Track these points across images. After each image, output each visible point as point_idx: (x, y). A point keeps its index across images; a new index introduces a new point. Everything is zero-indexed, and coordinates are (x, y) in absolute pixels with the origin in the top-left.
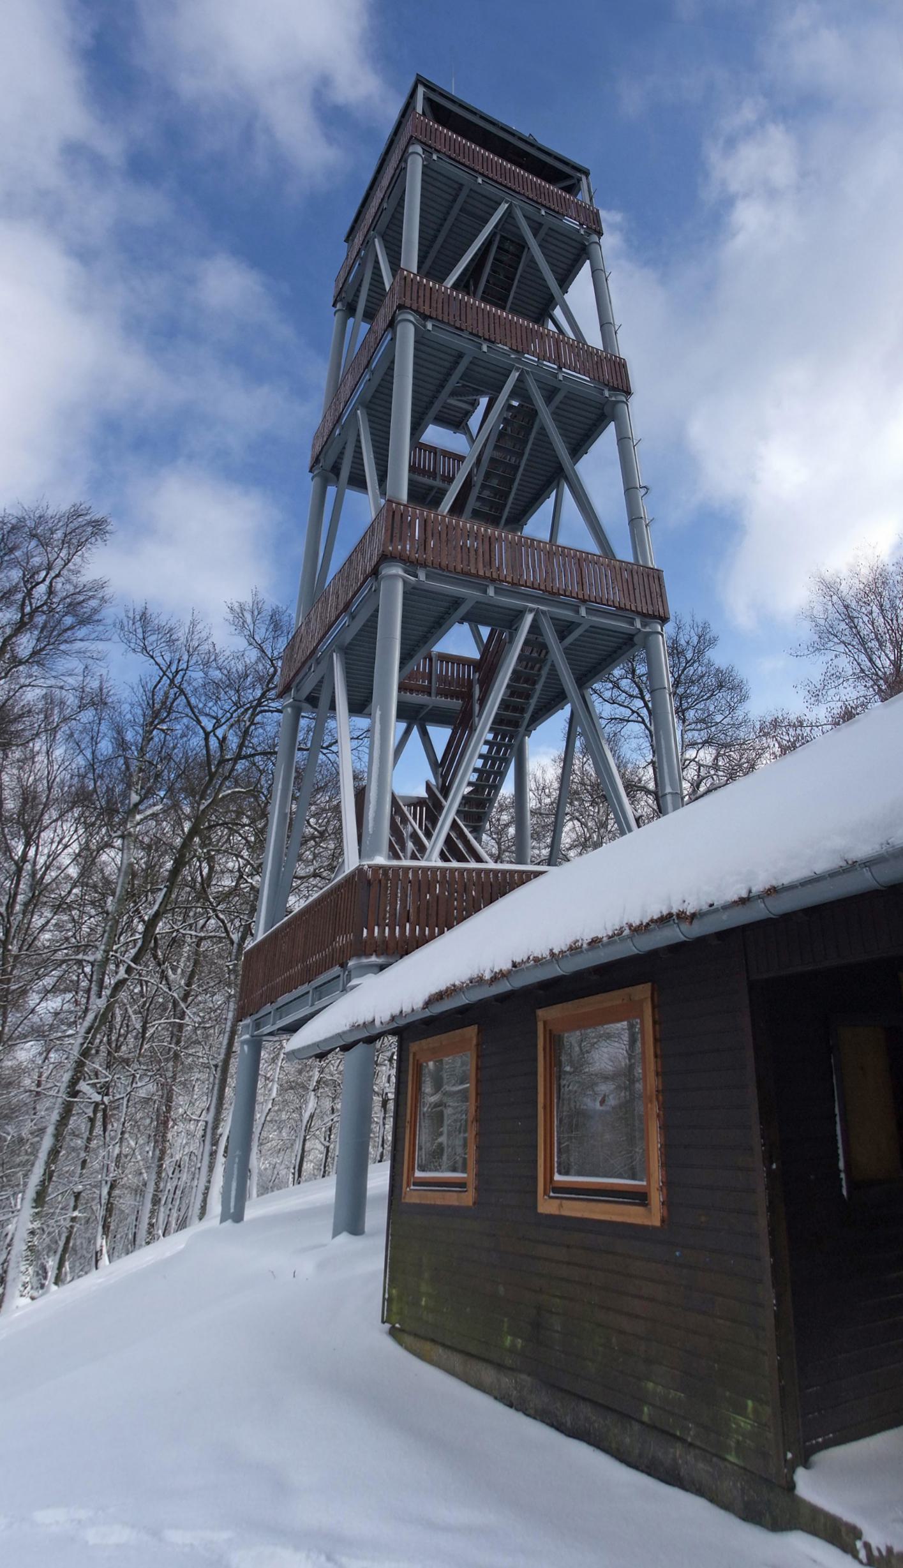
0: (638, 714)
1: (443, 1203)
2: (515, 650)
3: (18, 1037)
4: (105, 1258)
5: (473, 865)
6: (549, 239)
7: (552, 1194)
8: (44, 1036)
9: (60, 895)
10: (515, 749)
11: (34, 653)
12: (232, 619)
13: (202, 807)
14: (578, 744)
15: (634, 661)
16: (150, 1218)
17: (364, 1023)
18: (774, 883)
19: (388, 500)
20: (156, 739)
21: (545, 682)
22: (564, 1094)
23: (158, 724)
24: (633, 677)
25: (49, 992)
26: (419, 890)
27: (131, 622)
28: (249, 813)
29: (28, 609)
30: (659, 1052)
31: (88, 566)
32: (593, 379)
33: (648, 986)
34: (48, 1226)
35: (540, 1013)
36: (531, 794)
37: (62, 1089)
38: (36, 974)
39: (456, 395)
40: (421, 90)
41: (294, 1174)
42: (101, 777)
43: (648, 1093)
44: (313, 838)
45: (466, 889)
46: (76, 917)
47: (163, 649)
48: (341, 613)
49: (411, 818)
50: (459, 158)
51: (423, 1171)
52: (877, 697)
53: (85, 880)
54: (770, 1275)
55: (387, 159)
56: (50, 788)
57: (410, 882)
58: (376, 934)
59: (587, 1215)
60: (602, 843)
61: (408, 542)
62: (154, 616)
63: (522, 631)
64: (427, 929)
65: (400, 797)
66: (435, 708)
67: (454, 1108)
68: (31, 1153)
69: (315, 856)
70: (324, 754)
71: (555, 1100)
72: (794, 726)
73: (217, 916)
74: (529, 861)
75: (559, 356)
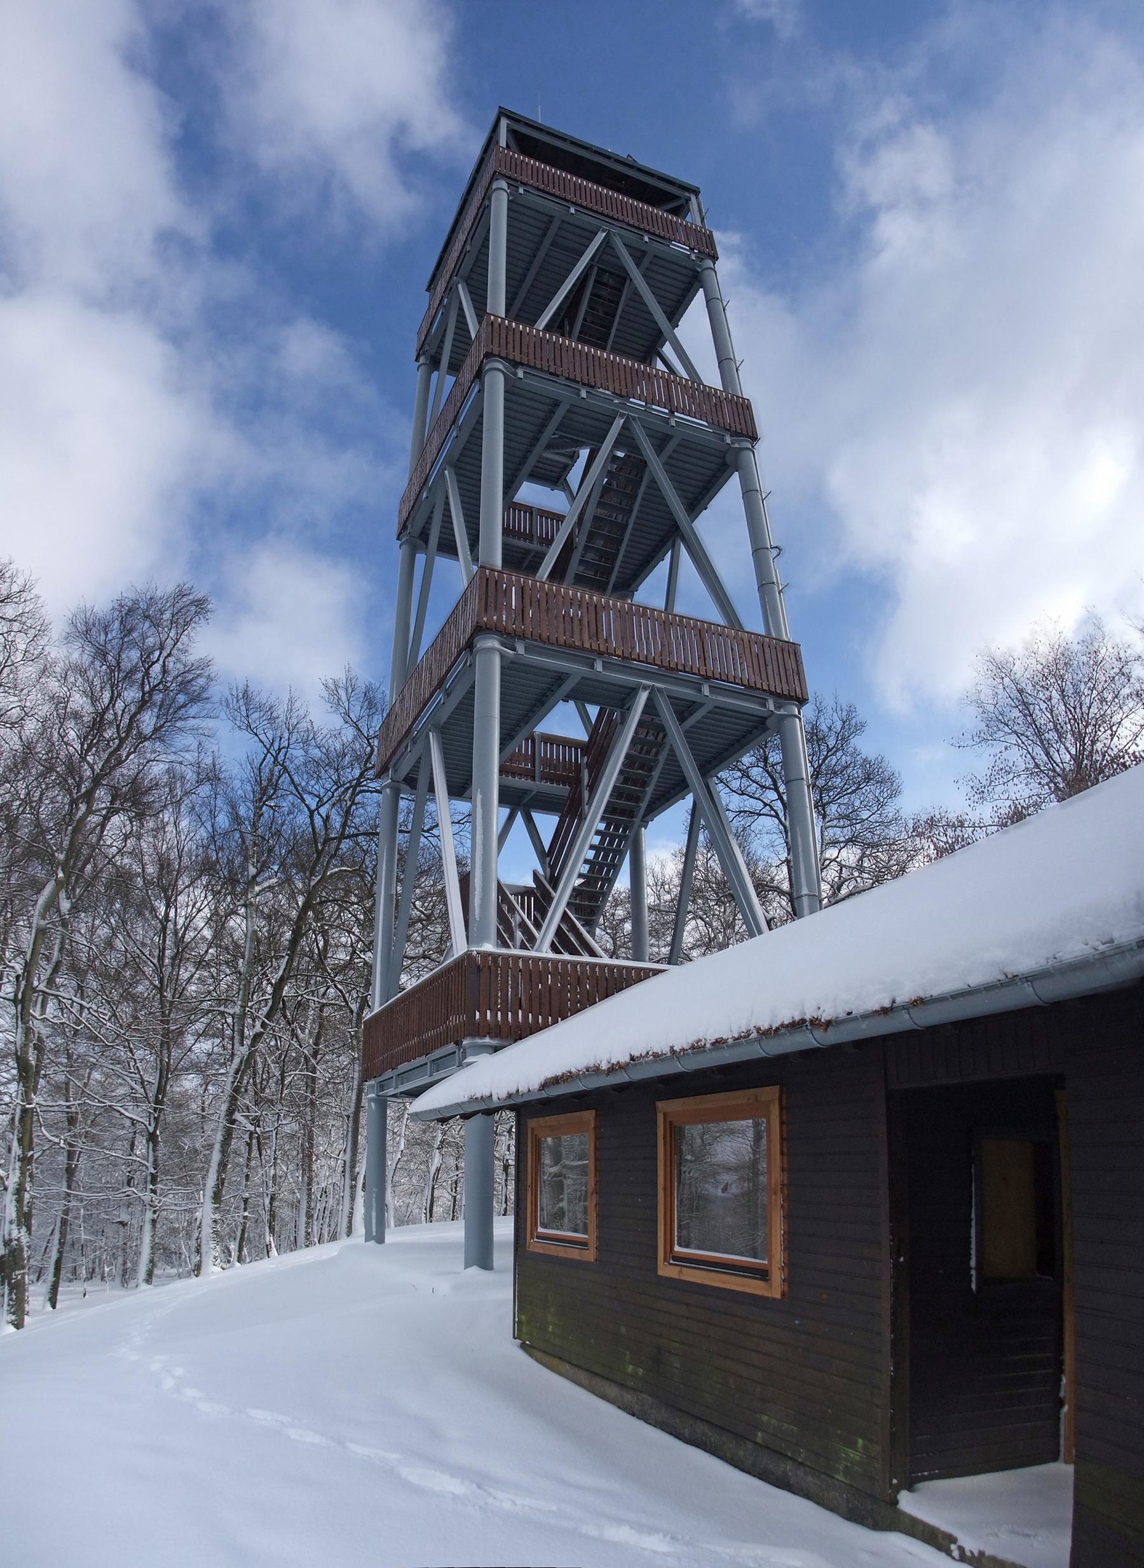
0: (771, 807)
1: (565, 1256)
3: (182, 1069)
4: (274, 1252)
5: (586, 958)
6: (655, 268)
7: (671, 1262)
8: (202, 1072)
9: (199, 953)
10: (630, 840)
11: (156, 730)
13: (313, 883)
16: (306, 1227)
17: (482, 1097)
18: (922, 994)
19: (481, 567)
20: (266, 815)
21: (663, 769)
22: (684, 1179)
23: (267, 800)
25: (200, 1035)
26: (530, 980)
27: (235, 700)
28: (357, 892)
29: (147, 688)
30: (785, 1150)
32: (711, 424)
34: (226, 1219)
35: (660, 1105)
37: (222, 1116)
38: (189, 1019)
40: (504, 123)
42: (221, 848)
43: (773, 1186)
44: (420, 920)
45: (579, 981)
47: (266, 727)
48: (435, 690)
49: (519, 908)
50: (550, 189)
51: (546, 1228)
52: (1052, 796)
53: (218, 942)
54: (889, 1347)
55: (469, 199)
56: (180, 857)
57: (520, 971)
58: (489, 1017)
60: (728, 944)
61: (504, 612)
62: (255, 694)
64: (540, 1017)
66: (539, 794)
69: (423, 938)
70: (426, 838)
71: (676, 1184)
74: (647, 958)
75: (670, 399)
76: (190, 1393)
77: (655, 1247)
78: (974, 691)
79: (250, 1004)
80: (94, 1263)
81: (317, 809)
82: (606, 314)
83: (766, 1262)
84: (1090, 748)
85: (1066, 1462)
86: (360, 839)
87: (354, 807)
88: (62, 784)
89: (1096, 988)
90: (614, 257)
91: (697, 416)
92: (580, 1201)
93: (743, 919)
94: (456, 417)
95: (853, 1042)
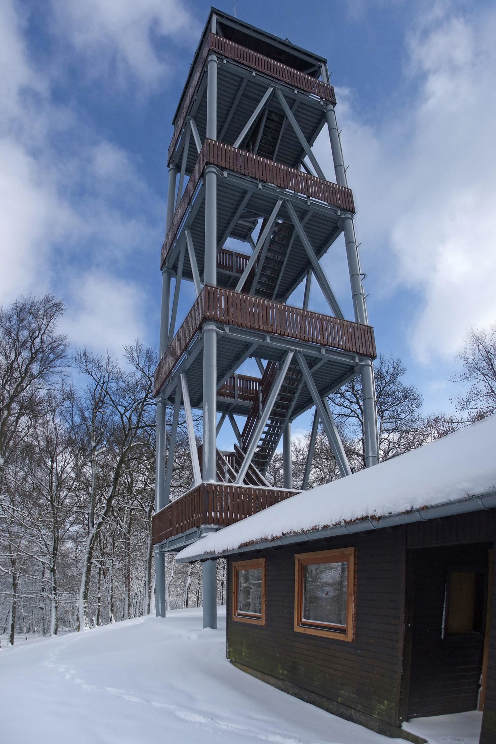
2: (283, 374)
4: (114, 621)
5: (261, 487)
6: (300, 110)
7: (301, 626)
10: (283, 429)
11: (40, 373)
13: (124, 450)
15: (354, 382)
18: (426, 504)
20: (98, 416)
23: (98, 409)
24: (353, 391)
25: (73, 523)
26: (233, 497)
27: (79, 357)
28: (146, 455)
29: (33, 351)
30: (356, 576)
31: (56, 328)
32: (330, 204)
35: (296, 556)
36: (292, 453)
40: (215, 17)
42: (77, 433)
43: (350, 592)
44: (178, 468)
45: (257, 498)
49: (227, 462)
50: (241, 60)
55: (195, 67)
56: (57, 437)
57: (228, 493)
58: (213, 515)
59: (317, 634)
60: (331, 480)
61: (218, 310)
62: (89, 354)
63: (287, 362)
69: (180, 477)
70: (180, 428)
72: (448, 422)
73: (137, 500)
74: (291, 487)
76: (78, 681)
79: (96, 509)
80: (30, 625)
81: (124, 413)
82: (273, 138)
86: (147, 428)
87: (143, 412)
92: (258, 599)
94: (190, 200)
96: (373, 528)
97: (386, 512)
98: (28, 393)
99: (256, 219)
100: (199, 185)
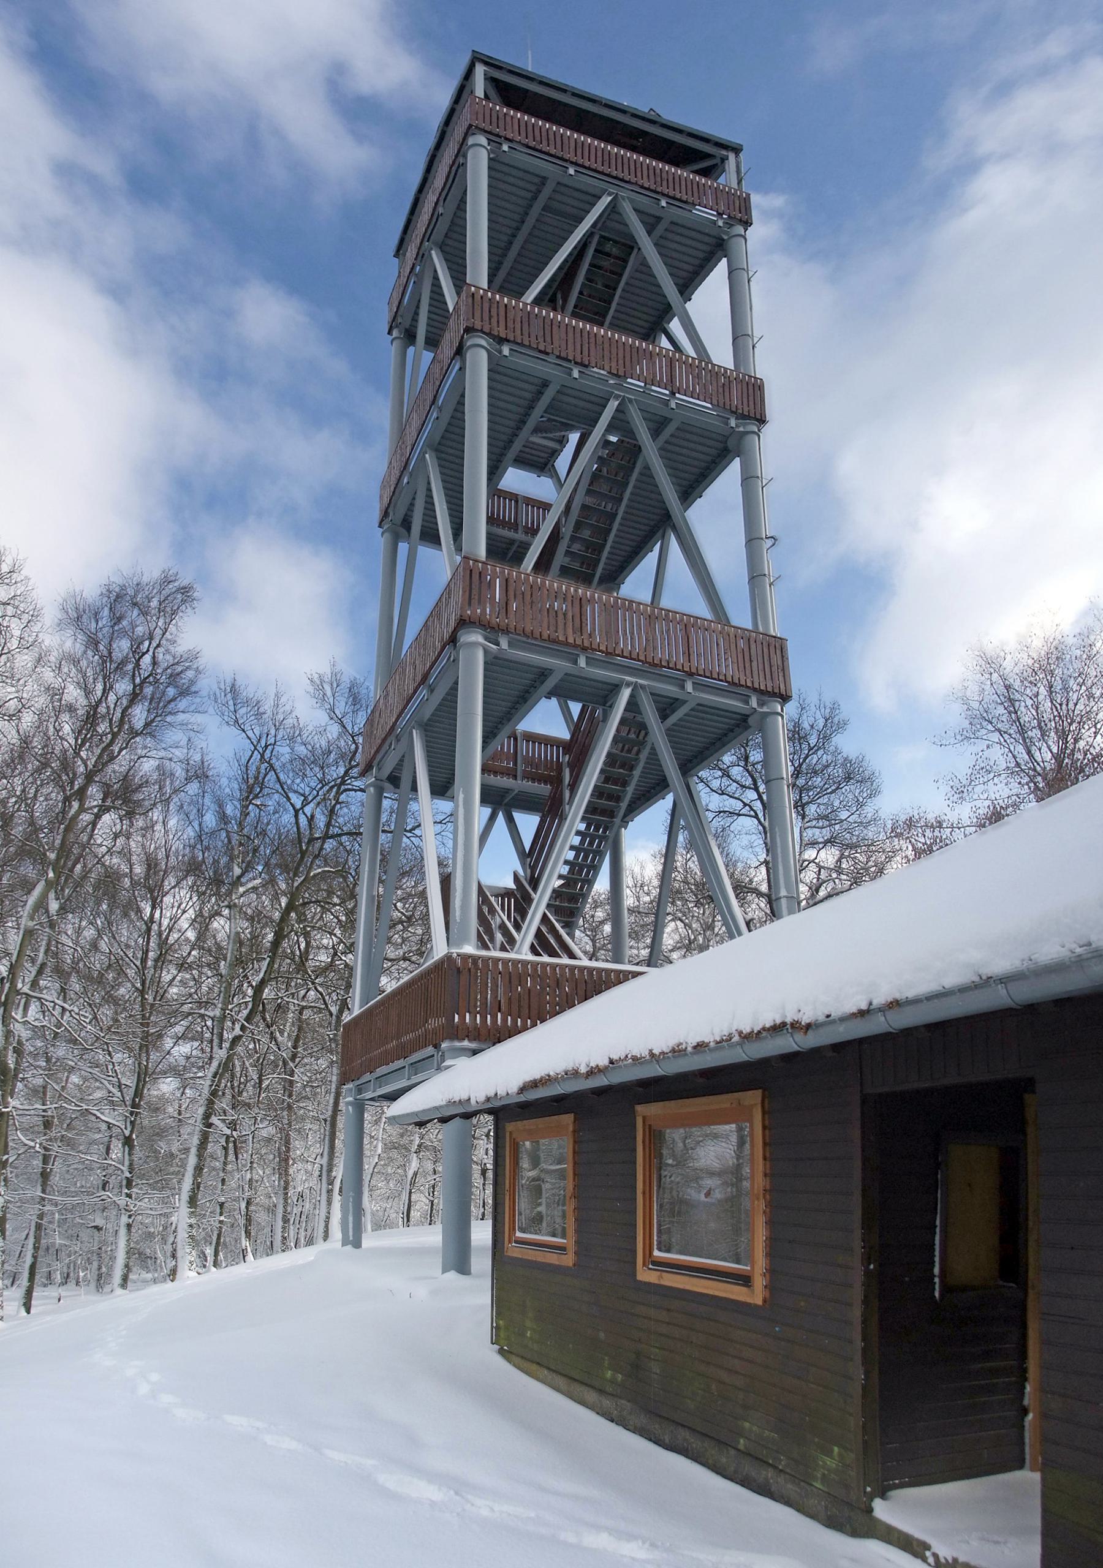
0: (750, 807)
2: (610, 731)
3: (160, 1073)
4: (250, 1257)
5: (565, 960)
6: (670, 236)
7: (651, 1266)
10: (610, 841)
11: (147, 725)
12: (312, 691)
13: (296, 884)
14: (681, 838)
15: (747, 746)
18: (898, 996)
19: (465, 557)
20: (252, 814)
21: (644, 768)
22: (665, 1183)
23: (253, 799)
24: (746, 765)
26: (510, 982)
27: (223, 694)
28: (339, 893)
29: (138, 681)
30: (768, 1155)
32: (716, 406)
33: (759, 1093)
35: (639, 1108)
36: (628, 891)
37: (199, 1120)
39: (541, 432)
40: (480, 70)
41: (403, 1218)
42: (207, 848)
43: (756, 1192)
44: (401, 922)
45: (558, 984)
46: (196, 977)
48: (419, 685)
49: (499, 909)
52: (1032, 796)
56: (167, 857)
57: (500, 973)
58: (467, 1020)
59: (688, 1287)
60: (708, 946)
62: (242, 688)
63: (618, 708)
65: (486, 886)
67: (552, 1184)
68: (181, 1166)
69: (404, 940)
73: (316, 988)
74: (627, 961)
76: (166, 1399)
77: (634, 1252)
78: (960, 688)
80: (69, 1268)
81: (302, 808)
82: (607, 286)
83: (749, 1268)
84: (1072, 746)
85: (1032, 1470)
86: (344, 838)
87: (338, 806)
88: (57, 780)
89: (1071, 991)
90: (620, 223)
91: (701, 397)
92: (558, 1205)
93: (723, 920)
94: (435, 397)
95: (831, 1045)
96: (796, 1048)
97: (820, 1014)
98: (121, 766)
99: (566, 434)
100: (453, 368)
